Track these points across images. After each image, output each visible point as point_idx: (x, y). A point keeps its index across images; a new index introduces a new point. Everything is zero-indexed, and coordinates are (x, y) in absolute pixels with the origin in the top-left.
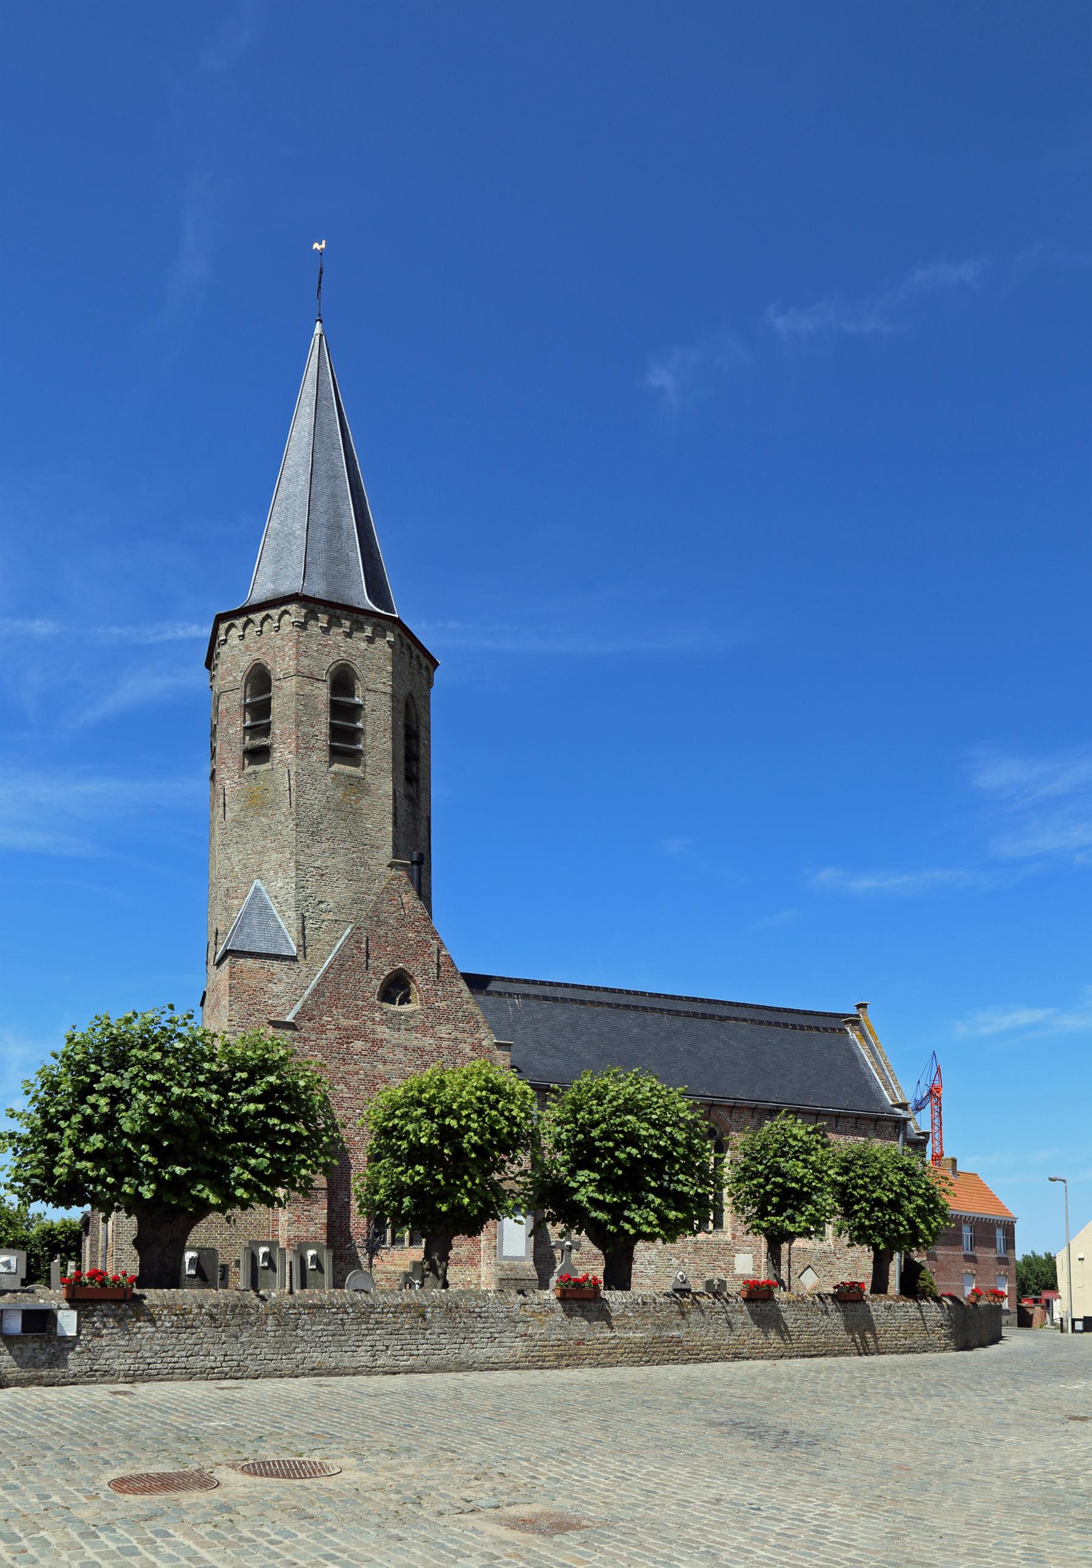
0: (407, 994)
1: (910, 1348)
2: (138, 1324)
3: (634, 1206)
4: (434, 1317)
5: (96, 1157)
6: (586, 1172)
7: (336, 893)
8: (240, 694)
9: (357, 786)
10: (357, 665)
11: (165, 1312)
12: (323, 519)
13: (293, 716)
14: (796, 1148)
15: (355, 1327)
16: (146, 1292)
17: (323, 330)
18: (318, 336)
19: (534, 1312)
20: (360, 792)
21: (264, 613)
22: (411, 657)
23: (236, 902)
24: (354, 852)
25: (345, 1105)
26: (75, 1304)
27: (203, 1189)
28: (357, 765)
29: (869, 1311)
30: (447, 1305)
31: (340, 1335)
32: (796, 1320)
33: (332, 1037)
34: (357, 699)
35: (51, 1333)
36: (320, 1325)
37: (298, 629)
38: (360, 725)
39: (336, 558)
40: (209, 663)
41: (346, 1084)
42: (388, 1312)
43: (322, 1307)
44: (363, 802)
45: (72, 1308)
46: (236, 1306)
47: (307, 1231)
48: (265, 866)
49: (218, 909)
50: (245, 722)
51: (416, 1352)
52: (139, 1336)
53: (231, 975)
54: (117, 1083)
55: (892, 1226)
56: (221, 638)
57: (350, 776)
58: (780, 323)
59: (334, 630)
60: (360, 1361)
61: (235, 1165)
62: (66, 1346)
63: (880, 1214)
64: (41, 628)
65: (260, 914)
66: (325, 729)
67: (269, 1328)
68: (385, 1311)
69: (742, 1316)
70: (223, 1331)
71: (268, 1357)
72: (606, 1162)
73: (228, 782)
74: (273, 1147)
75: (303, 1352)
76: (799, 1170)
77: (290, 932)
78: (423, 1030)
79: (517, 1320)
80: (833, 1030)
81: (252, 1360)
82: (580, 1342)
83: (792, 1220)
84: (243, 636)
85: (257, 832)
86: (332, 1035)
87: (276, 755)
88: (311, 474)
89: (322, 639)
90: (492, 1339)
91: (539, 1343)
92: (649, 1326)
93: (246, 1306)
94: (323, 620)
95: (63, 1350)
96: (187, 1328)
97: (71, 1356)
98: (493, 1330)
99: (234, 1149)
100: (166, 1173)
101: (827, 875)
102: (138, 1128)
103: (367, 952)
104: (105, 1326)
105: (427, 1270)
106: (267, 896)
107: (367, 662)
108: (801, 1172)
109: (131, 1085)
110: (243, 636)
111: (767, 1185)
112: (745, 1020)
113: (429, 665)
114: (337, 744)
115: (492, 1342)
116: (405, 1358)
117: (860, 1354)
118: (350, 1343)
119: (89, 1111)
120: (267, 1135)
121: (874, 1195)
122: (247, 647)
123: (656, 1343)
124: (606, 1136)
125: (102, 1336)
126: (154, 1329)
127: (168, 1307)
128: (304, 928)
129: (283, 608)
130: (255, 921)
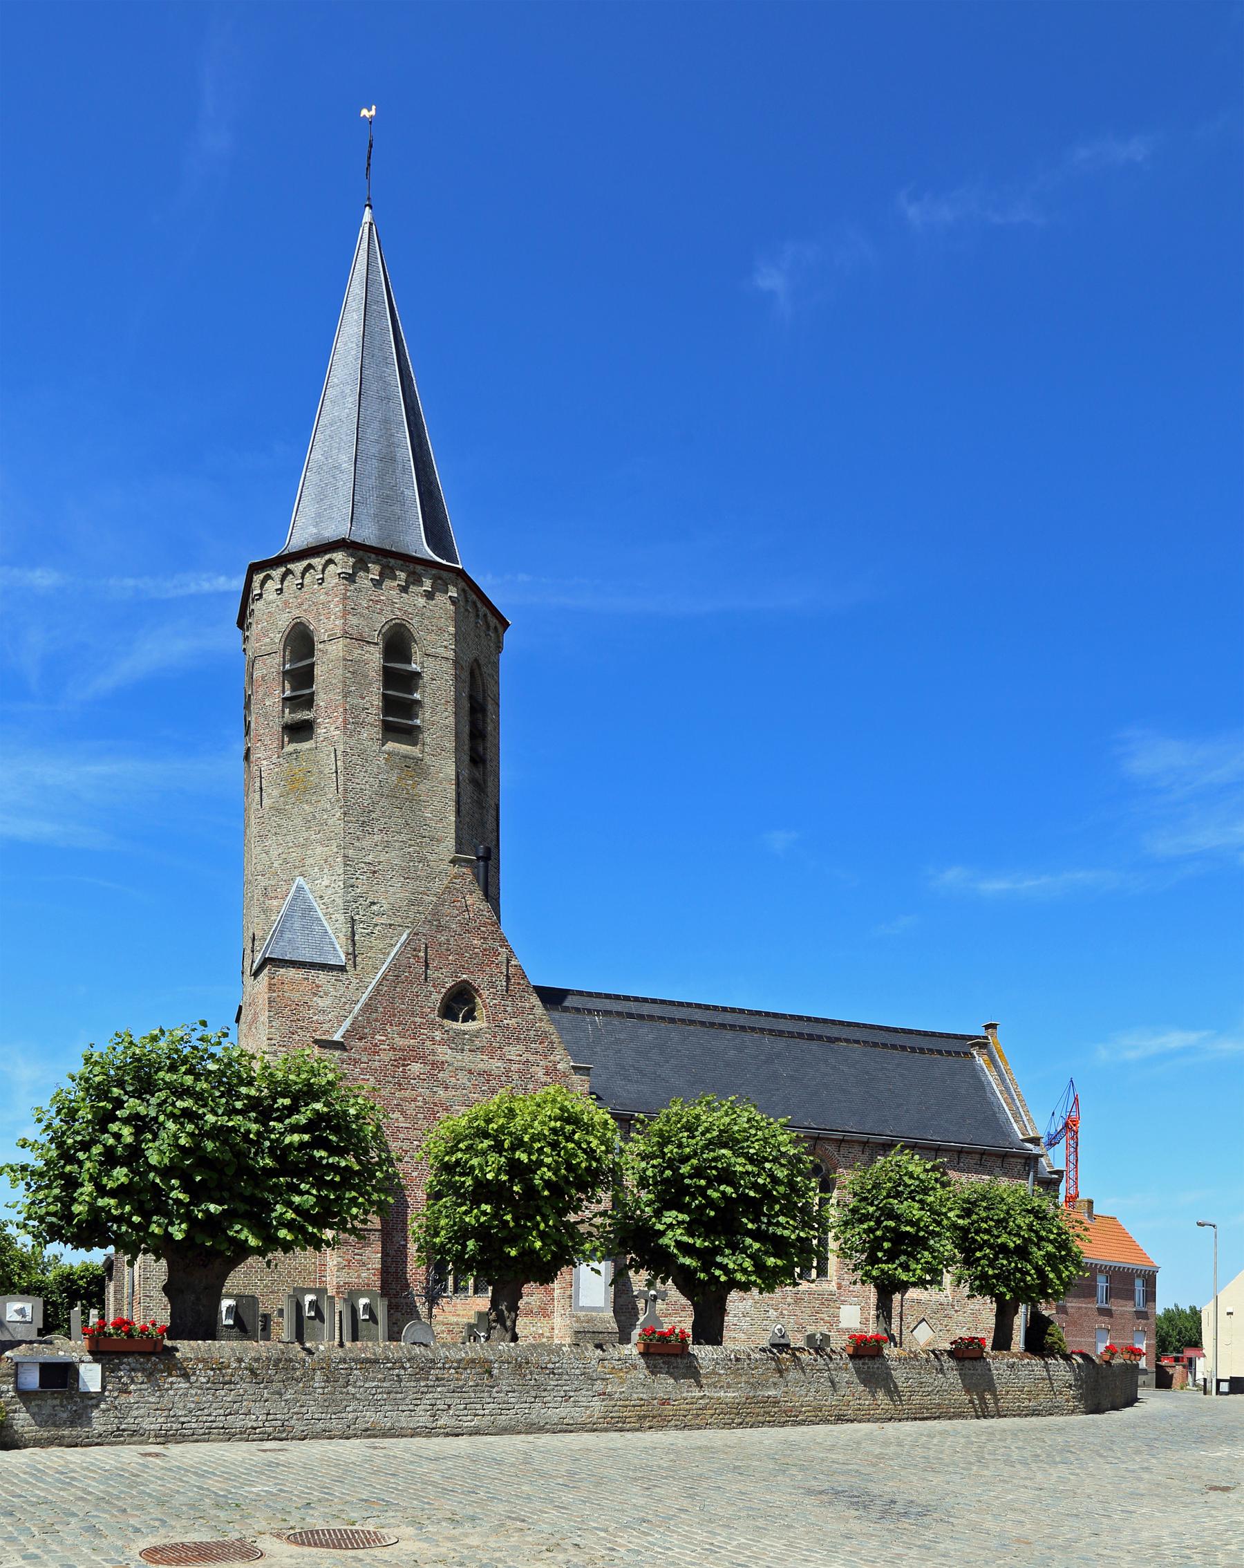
0: (472, 1010)
1: (1034, 1410)
2: (170, 1379)
3: (727, 1251)
4: (501, 1373)
5: (121, 1193)
6: (674, 1213)
7: (391, 893)
8: (278, 659)
9: (415, 768)
10: (414, 624)
11: (200, 1366)
12: (374, 450)
13: (340, 685)
14: (913, 1188)
15: (413, 1384)
16: (178, 1344)
17: (373, 218)
18: (368, 225)
19: (614, 1368)
20: (418, 775)
21: (305, 563)
22: (477, 616)
23: (275, 903)
24: (410, 846)
25: (401, 1136)
26: (99, 1357)
27: (241, 1230)
28: (414, 744)
29: (990, 1370)
30: (516, 1360)
31: (397, 1393)
32: (907, 1379)
33: (387, 1059)
34: (414, 666)
35: (72, 1389)
36: (373, 1381)
37: (345, 582)
38: (417, 696)
39: (390, 498)
40: (242, 622)
41: (402, 1112)
42: (450, 1368)
43: (376, 1361)
44: (421, 787)
45: (96, 1361)
46: (279, 1360)
47: (359, 1277)
48: (309, 861)
49: (255, 911)
50: (284, 693)
51: (481, 1412)
52: (171, 1392)
53: (271, 987)
54: (142, 1110)
55: (1018, 1275)
56: (255, 592)
57: (405, 757)
58: (913, 212)
59: (388, 583)
60: (418, 1422)
61: (277, 1203)
62: (90, 1403)
63: (1005, 1262)
64: (43, 579)
65: (303, 917)
66: (377, 702)
67: (317, 1385)
68: (447, 1366)
69: (847, 1375)
70: (266, 1388)
71: (316, 1416)
72: (697, 1202)
73: (265, 762)
74: (320, 1183)
75: (354, 1411)
76: (915, 1212)
77: (338, 937)
78: (490, 1050)
79: (595, 1377)
80: (958, 1053)
81: (298, 1420)
82: (664, 1402)
83: (906, 1268)
84: (281, 590)
85: (298, 821)
86: (386, 1056)
87: (320, 731)
88: (360, 394)
89: (374, 594)
90: (566, 1398)
91: (618, 1403)
92: (743, 1385)
93: (291, 1360)
94: (375, 569)
95: (86, 1407)
96: (225, 1383)
97: (95, 1413)
98: (567, 1388)
99: (275, 1185)
100: (199, 1211)
101: (953, 876)
102: (166, 1161)
103: (426, 961)
104: (133, 1382)
105: (494, 1321)
106: (311, 897)
107: (426, 622)
108: (918, 1214)
109: (158, 1112)
110: (281, 590)
111: (877, 1229)
112: (857, 1042)
113: (498, 626)
114: (391, 719)
115: (566, 1401)
116: (469, 1418)
117: (978, 1417)
118: (408, 1401)
119: (111, 1141)
120: (312, 1169)
121: (999, 1241)
122: (286, 603)
123: (750, 1404)
124: (698, 1173)
125: (130, 1393)
126: (187, 1385)
127: (204, 1360)
128: (353, 934)
129: (327, 557)
130: (297, 925)
